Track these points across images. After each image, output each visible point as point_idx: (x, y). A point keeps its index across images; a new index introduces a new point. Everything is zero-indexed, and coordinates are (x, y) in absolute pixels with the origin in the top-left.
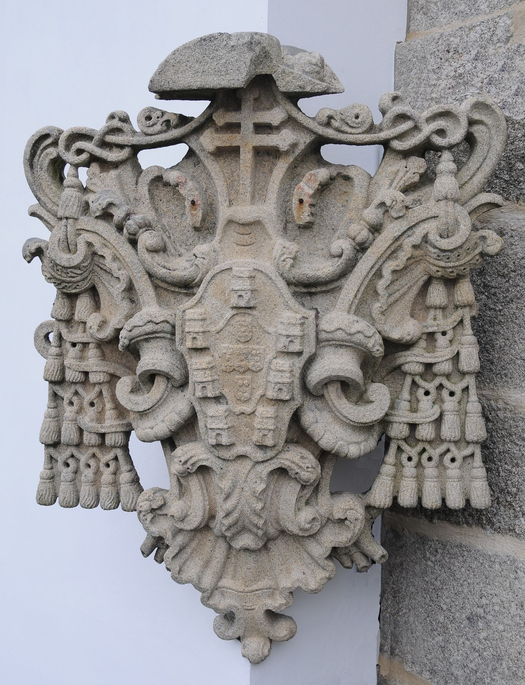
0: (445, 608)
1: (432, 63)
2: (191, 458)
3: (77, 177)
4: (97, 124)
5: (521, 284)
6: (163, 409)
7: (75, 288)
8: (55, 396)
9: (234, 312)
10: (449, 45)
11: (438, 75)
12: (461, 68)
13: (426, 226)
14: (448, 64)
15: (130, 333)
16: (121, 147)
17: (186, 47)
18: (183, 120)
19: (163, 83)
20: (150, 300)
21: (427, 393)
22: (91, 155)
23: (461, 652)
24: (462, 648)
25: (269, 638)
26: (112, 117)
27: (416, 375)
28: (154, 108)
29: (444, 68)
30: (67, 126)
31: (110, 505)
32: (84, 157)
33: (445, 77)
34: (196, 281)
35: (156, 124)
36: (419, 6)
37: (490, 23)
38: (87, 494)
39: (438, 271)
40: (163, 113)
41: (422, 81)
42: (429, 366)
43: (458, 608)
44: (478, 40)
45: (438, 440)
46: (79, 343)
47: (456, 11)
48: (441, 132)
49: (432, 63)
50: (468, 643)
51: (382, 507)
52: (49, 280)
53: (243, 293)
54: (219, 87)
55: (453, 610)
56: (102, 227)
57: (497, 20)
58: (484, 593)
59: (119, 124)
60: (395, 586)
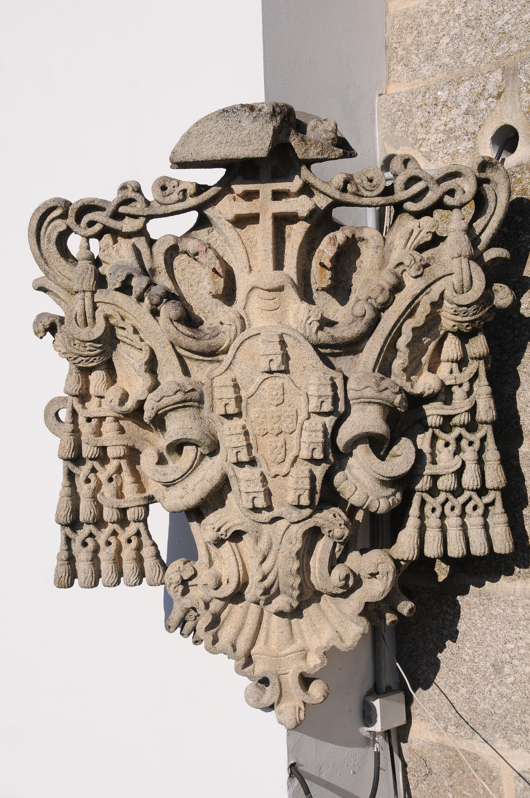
0: (467, 660)
1: (419, 117)
2: (225, 523)
3: (88, 248)
4: (110, 195)
5: (527, 333)
6: (193, 478)
7: (93, 362)
8: (71, 476)
9: (267, 375)
10: (436, 99)
11: (427, 129)
12: (451, 123)
13: (443, 283)
14: (436, 118)
15: (158, 404)
16: (135, 217)
17: (207, 118)
18: (201, 189)
19: (185, 154)
20: (175, 370)
21: (447, 445)
22: (105, 226)
23: (487, 700)
24: (489, 696)
25: (303, 702)
26: (124, 187)
27: (436, 427)
28: (168, 177)
29: (433, 121)
30: (76, 197)
31: (135, 581)
32: (97, 228)
33: (435, 131)
34: (223, 348)
35: (172, 193)
36: (399, 57)
37: (479, 78)
38: (110, 572)
39: (454, 326)
40: (179, 182)
41: (409, 135)
42: (448, 418)
43: (481, 657)
44: (468, 95)
45: (457, 492)
46: (94, 418)
47: (440, 63)
48: (451, 192)
49: (419, 117)
50: (495, 690)
51: (410, 559)
52: (63, 355)
53: (274, 357)
54: (242, 157)
55: (476, 660)
56: (120, 297)
57: (487, 75)
58: (509, 638)
59: (132, 195)
60: (411, 645)
